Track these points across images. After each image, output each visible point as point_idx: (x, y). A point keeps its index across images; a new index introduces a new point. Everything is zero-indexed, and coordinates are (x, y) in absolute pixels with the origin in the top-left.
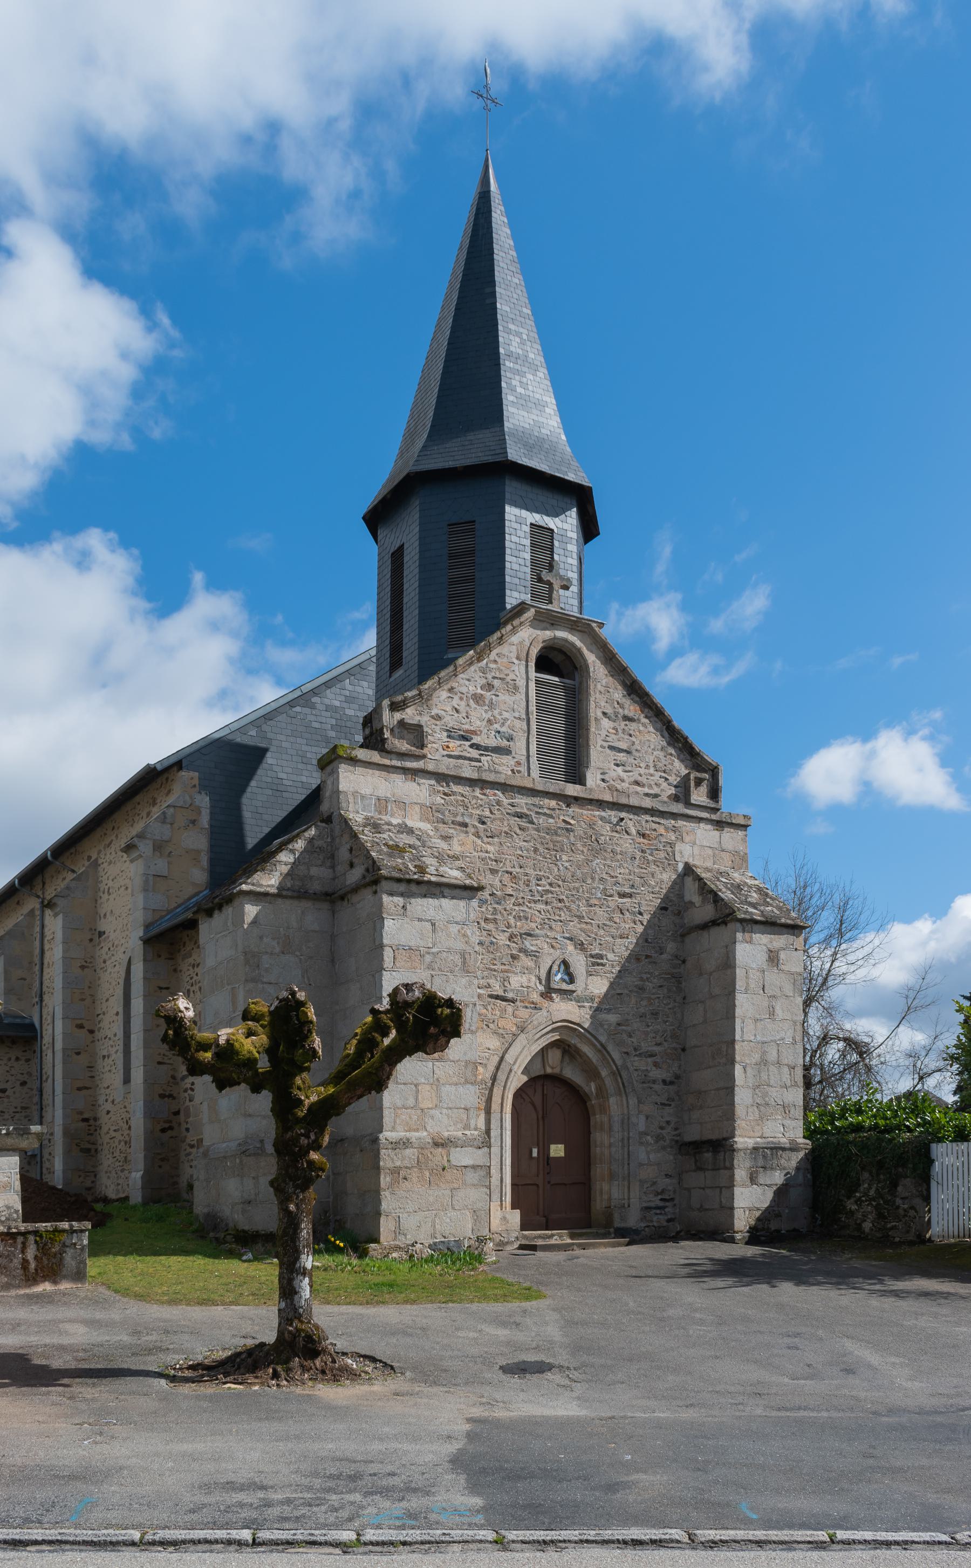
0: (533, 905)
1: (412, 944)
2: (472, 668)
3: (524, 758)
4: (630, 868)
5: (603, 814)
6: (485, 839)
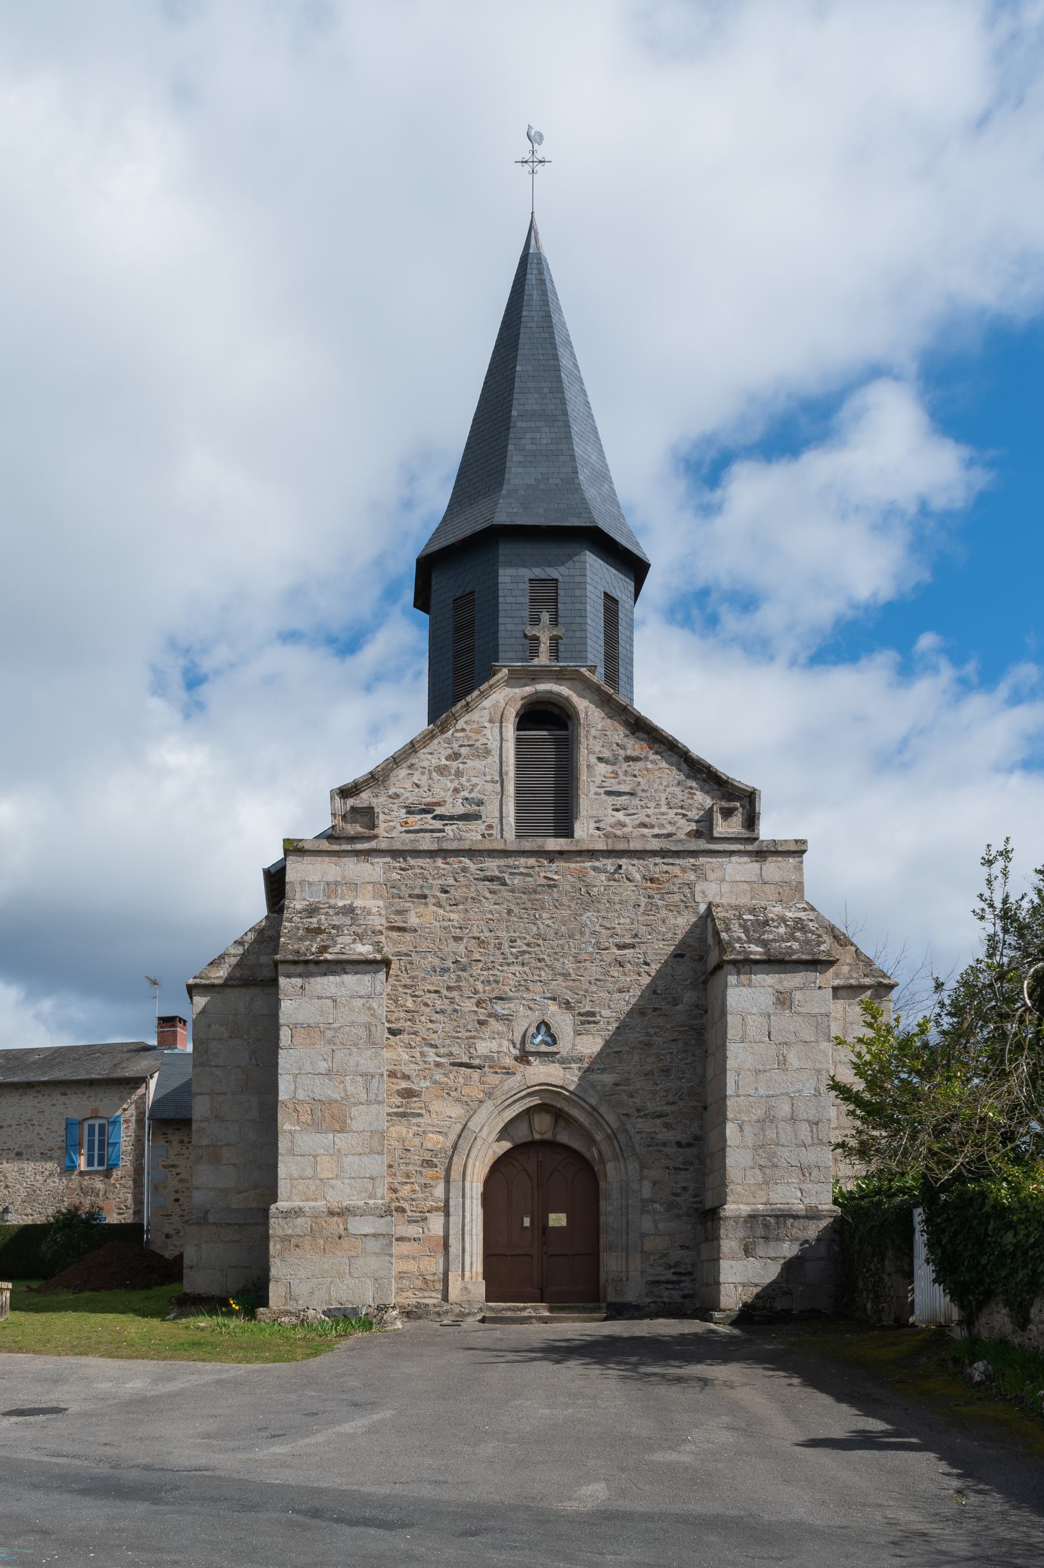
0: (505, 968)
1: (311, 1021)
2: (436, 741)
3: (497, 821)
4: (632, 916)
5: (597, 864)
6: (448, 908)
